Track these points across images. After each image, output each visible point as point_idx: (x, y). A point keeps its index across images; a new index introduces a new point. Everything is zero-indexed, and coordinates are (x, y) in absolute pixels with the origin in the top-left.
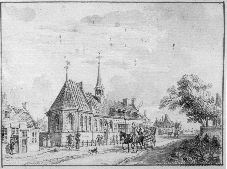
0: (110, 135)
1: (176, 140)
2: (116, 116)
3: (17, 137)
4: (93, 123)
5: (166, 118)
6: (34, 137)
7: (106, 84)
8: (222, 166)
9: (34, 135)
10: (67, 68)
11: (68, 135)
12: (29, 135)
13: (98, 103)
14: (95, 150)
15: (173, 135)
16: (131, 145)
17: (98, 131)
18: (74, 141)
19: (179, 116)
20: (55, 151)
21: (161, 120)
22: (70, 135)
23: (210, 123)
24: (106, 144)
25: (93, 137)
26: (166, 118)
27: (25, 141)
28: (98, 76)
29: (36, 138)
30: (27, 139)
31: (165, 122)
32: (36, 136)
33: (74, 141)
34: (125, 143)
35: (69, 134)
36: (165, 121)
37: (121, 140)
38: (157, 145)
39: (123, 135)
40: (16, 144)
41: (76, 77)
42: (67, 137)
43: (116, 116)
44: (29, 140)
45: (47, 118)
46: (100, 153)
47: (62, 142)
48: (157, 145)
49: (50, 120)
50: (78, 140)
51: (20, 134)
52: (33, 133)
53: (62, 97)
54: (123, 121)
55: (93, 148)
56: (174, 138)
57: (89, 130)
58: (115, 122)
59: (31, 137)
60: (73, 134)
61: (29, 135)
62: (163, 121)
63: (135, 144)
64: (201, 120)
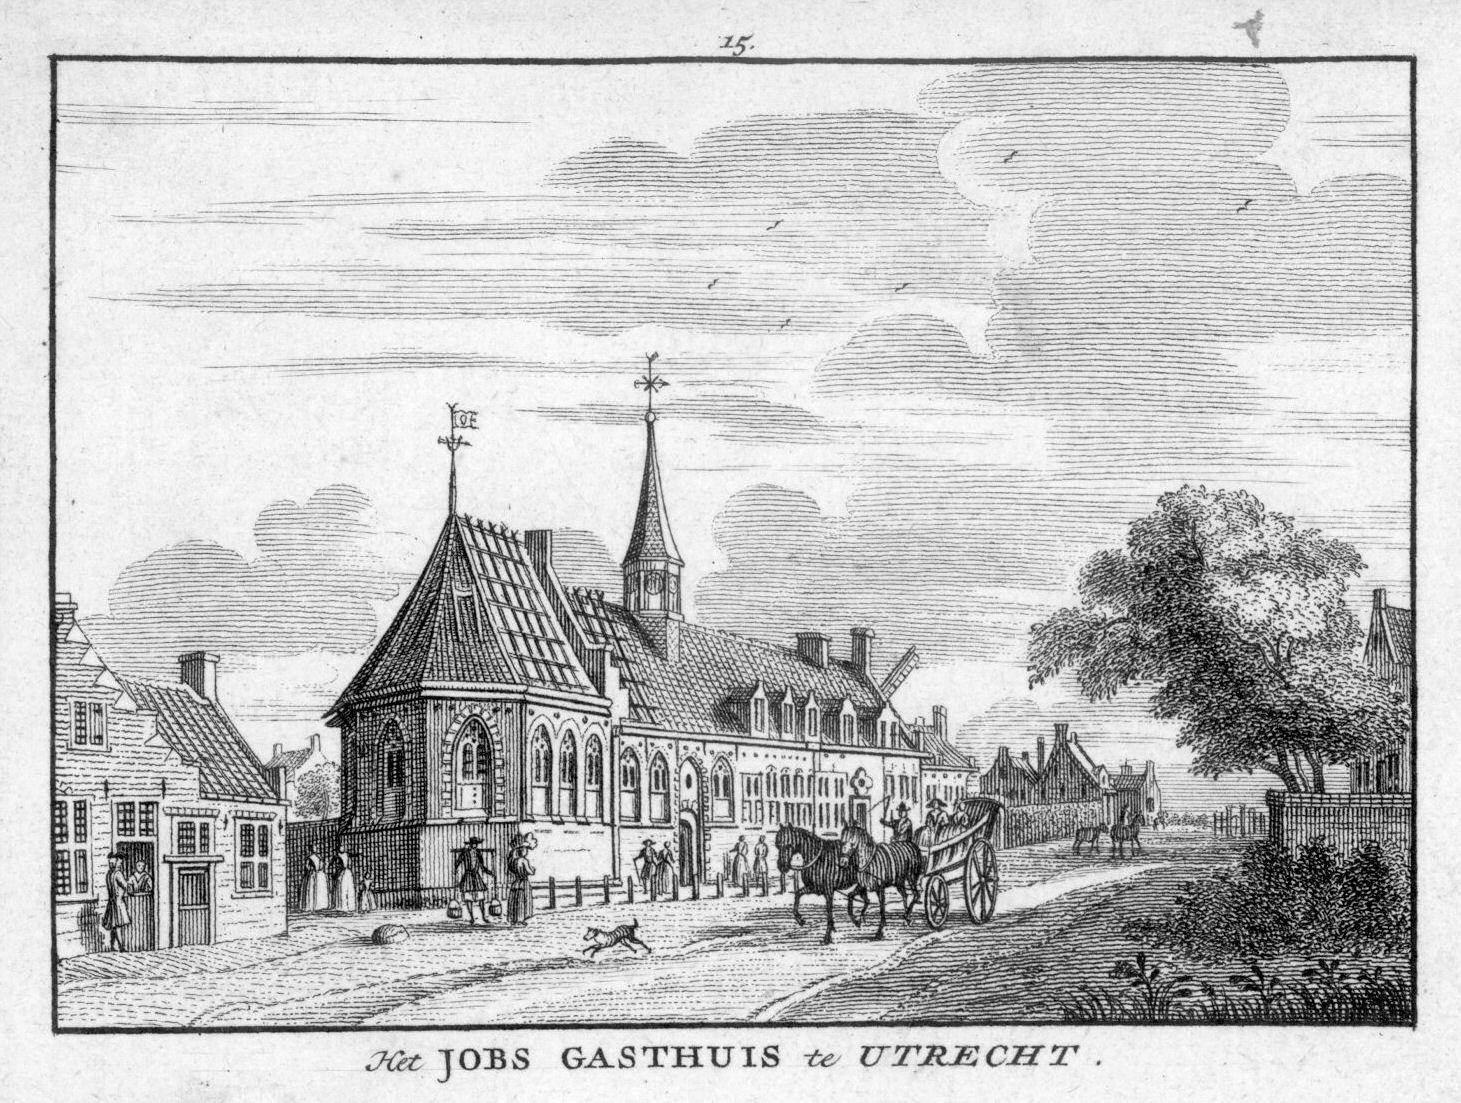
0: (719, 845)
1: (1125, 873)
2: (762, 727)
3: (146, 851)
4: (455, 233)
5: (1062, 746)
6: (257, 859)
7: (695, 542)
8: (1405, 1031)
9: (252, 839)
10: (452, 444)
11: (459, 838)
12: (225, 841)
13: (653, 664)
14: (627, 935)
15: (1105, 840)
16: (844, 903)
17: (645, 821)
18: (496, 882)
19: (1137, 735)
20: (377, 939)
21: (1034, 763)
22: (474, 841)
23: (1338, 777)
24: (694, 893)
25: (614, 857)
26: (1062, 746)
27: (197, 881)
28: (645, 492)
29: (264, 866)
30: (207, 870)
31: (1054, 768)
32: (264, 852)
33: (496, 882)
34: (811, 887)
35: (465, 835)
36: (1060, 768)
37: (784, 866)
38: (1010, 900)
39: (794, 840)
40: (138, 903)
41: (501, 497)
42: (455, 851)
43: (762, 727)
44: (223, 880)
45: (332, 742)
46: (658, 952)
47: (543, 790)
48: (1010, 900)
49: (352, 751)
50: (519, 874)
51: (166, 843)
52: (247, 831)
53: (432, 620)
54: (803, 763)
55: (613, 917)
56: (1117, 858)
57: (588, 804)
58: (750, 762)
59: (471, 781)
60: (491, 839)
61: (225, 841)
62: (1040, 762)
63: (873, 897)
64: (1282, 757)
